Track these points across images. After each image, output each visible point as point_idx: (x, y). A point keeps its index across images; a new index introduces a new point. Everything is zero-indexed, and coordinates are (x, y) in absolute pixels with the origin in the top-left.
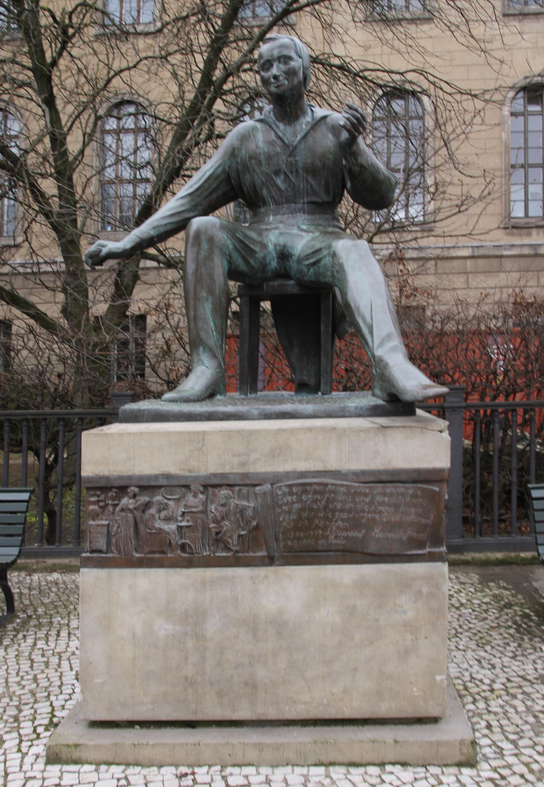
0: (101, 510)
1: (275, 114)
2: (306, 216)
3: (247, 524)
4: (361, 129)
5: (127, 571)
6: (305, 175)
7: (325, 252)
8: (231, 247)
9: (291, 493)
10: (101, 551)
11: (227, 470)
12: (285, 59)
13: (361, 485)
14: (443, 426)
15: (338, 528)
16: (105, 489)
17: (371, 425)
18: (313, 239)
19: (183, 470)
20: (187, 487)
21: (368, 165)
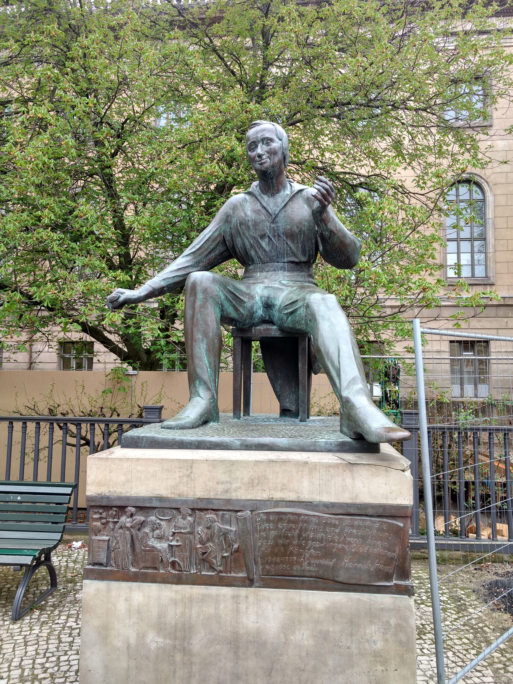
0: (103, 526)
1: (260, 188)
2: (286, 273)
3: (229, 546)
4: (330, 199)
5: (124, 585)
6: (285, 238)
7: (300, 304)
8: (223, 297)
9: (268, 521)
10: (101, 564)
11: (212, 495)
12: (268, 141)
13: (331, 516)
14: (406, 465)
15: (311, 556)
16: (107, 508)
17: (339, 461)
18: (290, 293)
19: (174, 493)
20: (178, 509)
21: (337, 230)
